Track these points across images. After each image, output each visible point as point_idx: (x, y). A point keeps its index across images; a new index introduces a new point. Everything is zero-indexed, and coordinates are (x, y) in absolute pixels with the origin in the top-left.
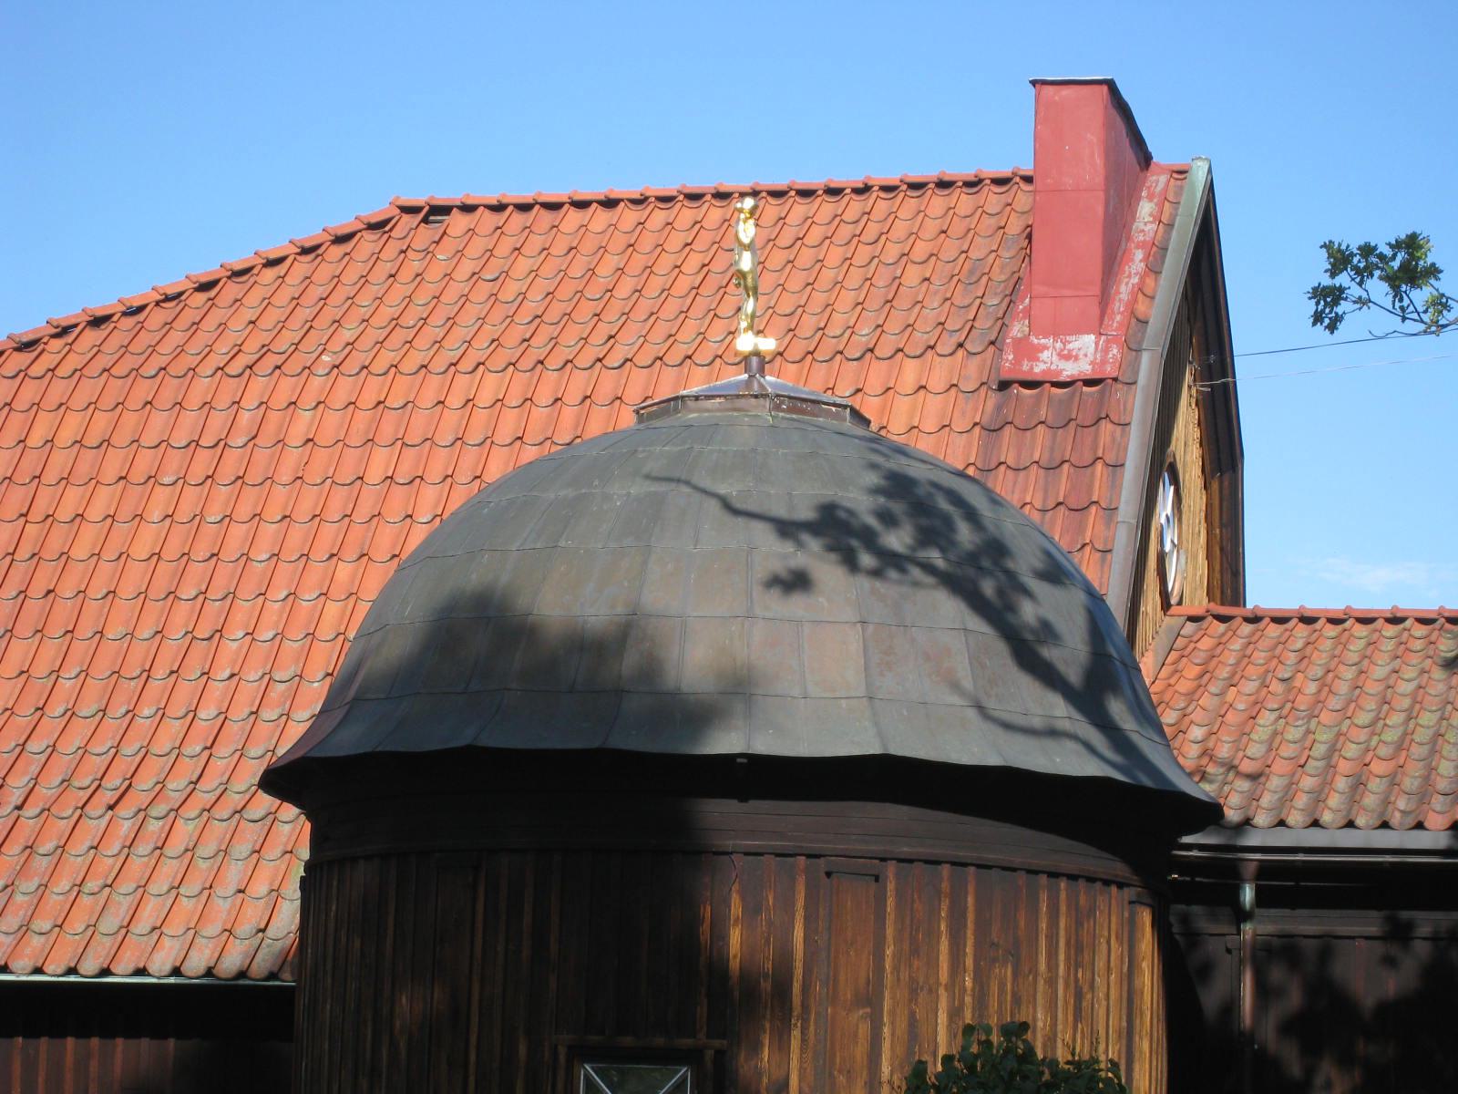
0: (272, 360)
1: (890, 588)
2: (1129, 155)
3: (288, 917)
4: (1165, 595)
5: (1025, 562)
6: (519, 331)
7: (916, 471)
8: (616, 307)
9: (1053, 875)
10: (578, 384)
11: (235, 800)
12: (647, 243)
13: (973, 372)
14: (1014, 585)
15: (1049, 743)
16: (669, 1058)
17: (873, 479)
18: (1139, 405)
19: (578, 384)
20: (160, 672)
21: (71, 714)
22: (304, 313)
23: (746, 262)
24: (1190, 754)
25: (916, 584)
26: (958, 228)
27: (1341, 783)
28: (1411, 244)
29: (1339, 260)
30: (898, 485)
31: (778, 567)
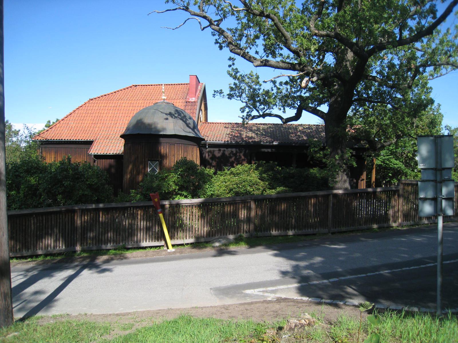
0: (121, 99)
1: (176, 120)
2: (198, 82)
3: (123, 149)
4: (201, 121)
5: (188, 117)
6: (143, 97)
7: (178, 109)
8: (152, 95)
9: (190, 145)
10: (149, 101)
11: (118, 138)
12: (155, 89)
13: (184, 101)
14: (187, 119)
15: (190, 133)
16: (156, 161)
17: (174, 110)
18: (198, 104)
19: (149, 101)
20: (111, 127)
21: (103, 131)
22: (124, 95)
23: (163, 90)
24: (202, 135)
26: (183, 88)
27: (215, 137)
28: (221, 90)
29: (215, 91)
30: (177, 111)
31: (166, 118)
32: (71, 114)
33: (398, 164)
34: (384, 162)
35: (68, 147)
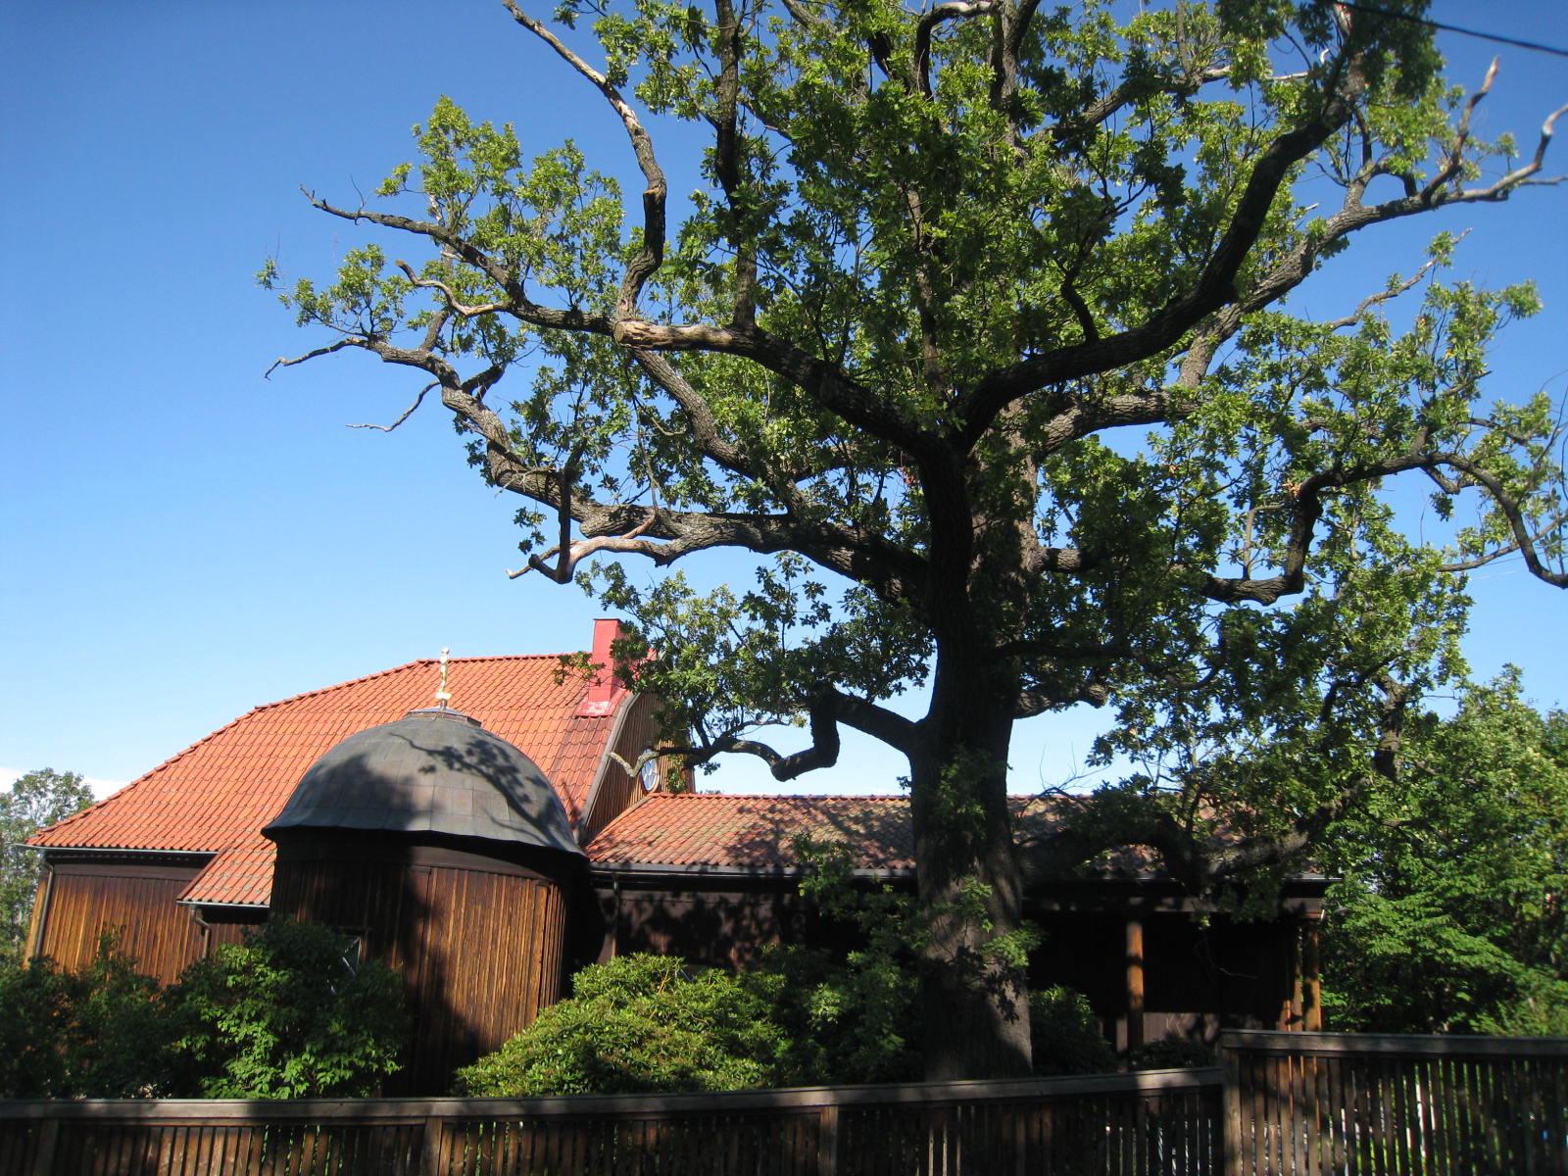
7: (488, 739)
9: (509, 875)
25: (539, 782)
32: (181, 757)
33: (1477, 953)
34: (1412, 944)
35: (136, 874)
